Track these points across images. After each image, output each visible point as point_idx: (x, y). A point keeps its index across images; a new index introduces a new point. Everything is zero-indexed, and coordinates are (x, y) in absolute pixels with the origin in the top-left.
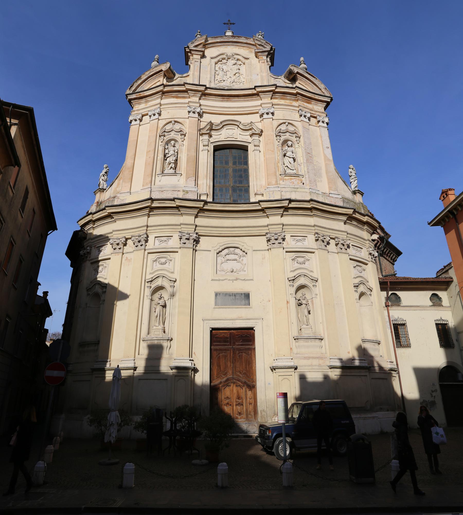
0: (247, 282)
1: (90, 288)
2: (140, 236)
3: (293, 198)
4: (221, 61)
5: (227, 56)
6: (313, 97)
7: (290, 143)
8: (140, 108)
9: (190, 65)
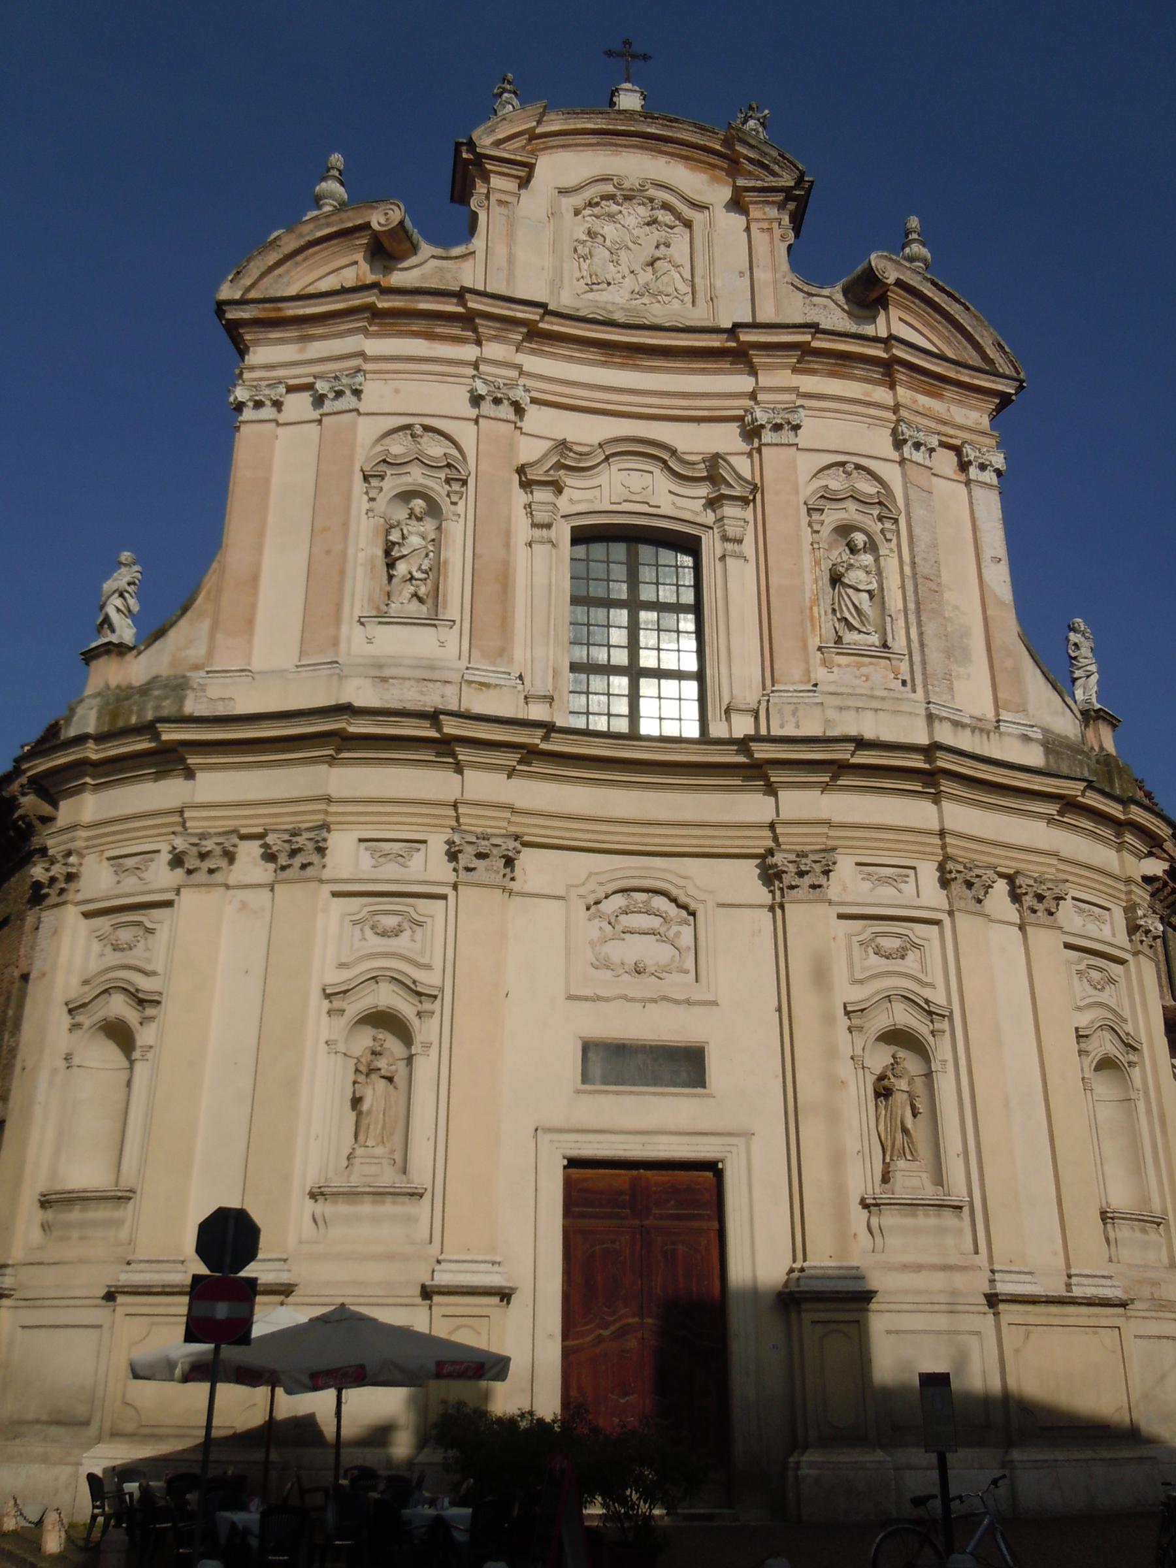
0: (697, 1010)
1: (84, 1005)
2: (295, 833)
3: (869, 734)
4: (597, 204)
5: (619, 187)
6: (952, 375)
7: (859, 538)
8: (268, 354)
9: (475, 215)
